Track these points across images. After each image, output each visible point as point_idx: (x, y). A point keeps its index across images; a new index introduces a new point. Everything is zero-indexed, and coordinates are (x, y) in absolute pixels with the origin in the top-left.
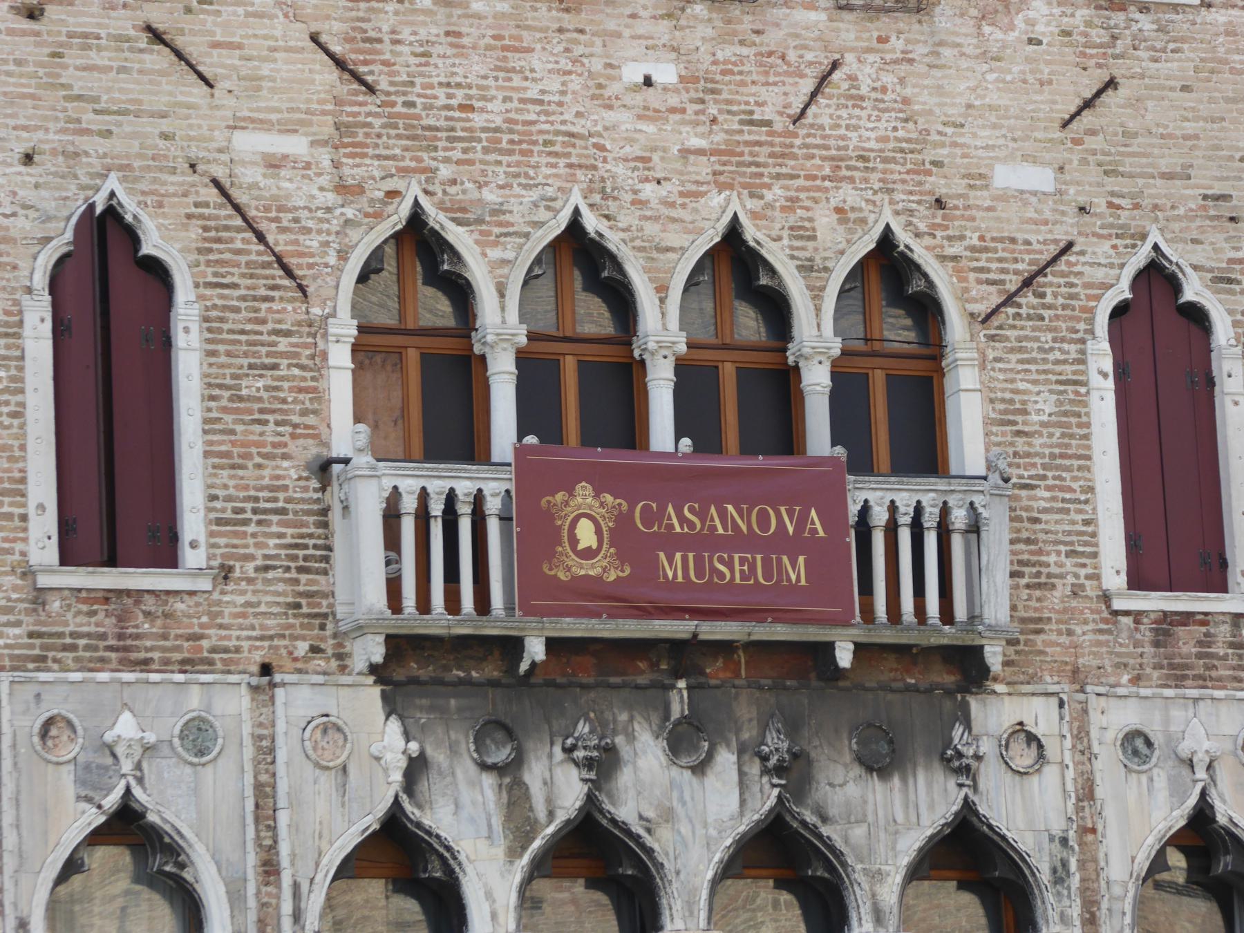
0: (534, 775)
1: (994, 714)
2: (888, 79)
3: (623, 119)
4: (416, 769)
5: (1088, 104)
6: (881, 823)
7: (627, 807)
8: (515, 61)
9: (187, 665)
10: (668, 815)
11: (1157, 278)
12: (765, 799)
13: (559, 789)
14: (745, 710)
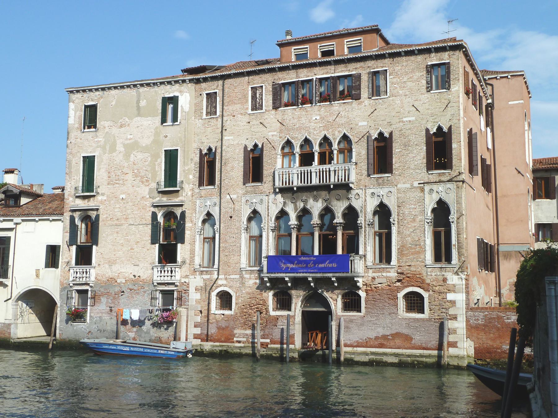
0: (298, 204)
1: (354, 192)
3: (312, 124)
6: (339, 208)
7: (308, 207)
8: (300, 119)
10: (313, 207)
13: (301, 205)
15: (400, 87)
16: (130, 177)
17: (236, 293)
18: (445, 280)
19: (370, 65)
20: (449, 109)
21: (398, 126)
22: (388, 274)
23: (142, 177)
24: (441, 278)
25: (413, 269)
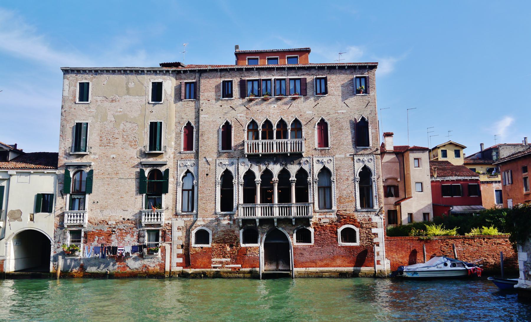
4: (251, 165)
6: (293, 169)
11: (322, 120)
12: (282, 168)
14: (281, 160)
15: (335, 90)
16: (120, 141)
17: (213, 231)
18: (370, 219)
19: (313, 73)
20: (369, 107)
21: (334, 115)
22: (330, 216)
23: (131, 142)
24: (367, 218)
25: (348, 212)
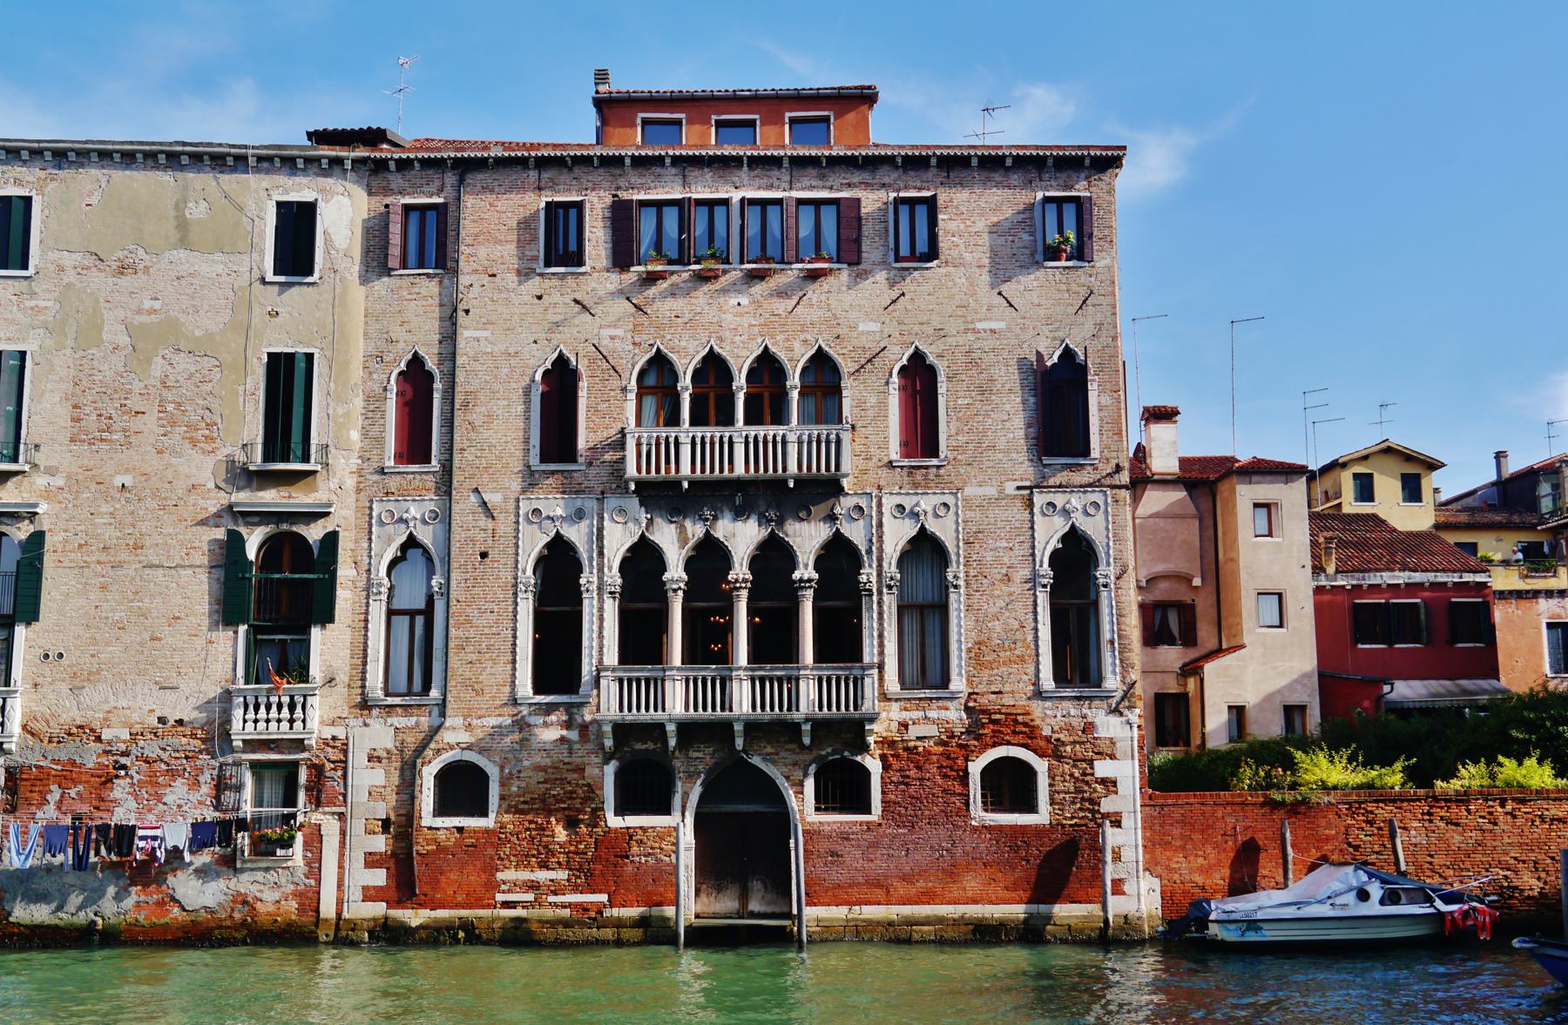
2: (823, 298)
5: (894, 302)
9: (577, 492)
11: (918, 357)
